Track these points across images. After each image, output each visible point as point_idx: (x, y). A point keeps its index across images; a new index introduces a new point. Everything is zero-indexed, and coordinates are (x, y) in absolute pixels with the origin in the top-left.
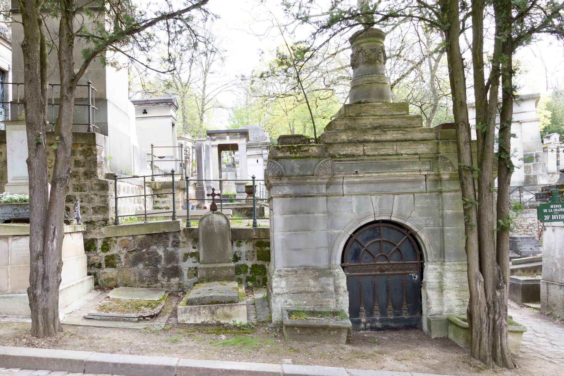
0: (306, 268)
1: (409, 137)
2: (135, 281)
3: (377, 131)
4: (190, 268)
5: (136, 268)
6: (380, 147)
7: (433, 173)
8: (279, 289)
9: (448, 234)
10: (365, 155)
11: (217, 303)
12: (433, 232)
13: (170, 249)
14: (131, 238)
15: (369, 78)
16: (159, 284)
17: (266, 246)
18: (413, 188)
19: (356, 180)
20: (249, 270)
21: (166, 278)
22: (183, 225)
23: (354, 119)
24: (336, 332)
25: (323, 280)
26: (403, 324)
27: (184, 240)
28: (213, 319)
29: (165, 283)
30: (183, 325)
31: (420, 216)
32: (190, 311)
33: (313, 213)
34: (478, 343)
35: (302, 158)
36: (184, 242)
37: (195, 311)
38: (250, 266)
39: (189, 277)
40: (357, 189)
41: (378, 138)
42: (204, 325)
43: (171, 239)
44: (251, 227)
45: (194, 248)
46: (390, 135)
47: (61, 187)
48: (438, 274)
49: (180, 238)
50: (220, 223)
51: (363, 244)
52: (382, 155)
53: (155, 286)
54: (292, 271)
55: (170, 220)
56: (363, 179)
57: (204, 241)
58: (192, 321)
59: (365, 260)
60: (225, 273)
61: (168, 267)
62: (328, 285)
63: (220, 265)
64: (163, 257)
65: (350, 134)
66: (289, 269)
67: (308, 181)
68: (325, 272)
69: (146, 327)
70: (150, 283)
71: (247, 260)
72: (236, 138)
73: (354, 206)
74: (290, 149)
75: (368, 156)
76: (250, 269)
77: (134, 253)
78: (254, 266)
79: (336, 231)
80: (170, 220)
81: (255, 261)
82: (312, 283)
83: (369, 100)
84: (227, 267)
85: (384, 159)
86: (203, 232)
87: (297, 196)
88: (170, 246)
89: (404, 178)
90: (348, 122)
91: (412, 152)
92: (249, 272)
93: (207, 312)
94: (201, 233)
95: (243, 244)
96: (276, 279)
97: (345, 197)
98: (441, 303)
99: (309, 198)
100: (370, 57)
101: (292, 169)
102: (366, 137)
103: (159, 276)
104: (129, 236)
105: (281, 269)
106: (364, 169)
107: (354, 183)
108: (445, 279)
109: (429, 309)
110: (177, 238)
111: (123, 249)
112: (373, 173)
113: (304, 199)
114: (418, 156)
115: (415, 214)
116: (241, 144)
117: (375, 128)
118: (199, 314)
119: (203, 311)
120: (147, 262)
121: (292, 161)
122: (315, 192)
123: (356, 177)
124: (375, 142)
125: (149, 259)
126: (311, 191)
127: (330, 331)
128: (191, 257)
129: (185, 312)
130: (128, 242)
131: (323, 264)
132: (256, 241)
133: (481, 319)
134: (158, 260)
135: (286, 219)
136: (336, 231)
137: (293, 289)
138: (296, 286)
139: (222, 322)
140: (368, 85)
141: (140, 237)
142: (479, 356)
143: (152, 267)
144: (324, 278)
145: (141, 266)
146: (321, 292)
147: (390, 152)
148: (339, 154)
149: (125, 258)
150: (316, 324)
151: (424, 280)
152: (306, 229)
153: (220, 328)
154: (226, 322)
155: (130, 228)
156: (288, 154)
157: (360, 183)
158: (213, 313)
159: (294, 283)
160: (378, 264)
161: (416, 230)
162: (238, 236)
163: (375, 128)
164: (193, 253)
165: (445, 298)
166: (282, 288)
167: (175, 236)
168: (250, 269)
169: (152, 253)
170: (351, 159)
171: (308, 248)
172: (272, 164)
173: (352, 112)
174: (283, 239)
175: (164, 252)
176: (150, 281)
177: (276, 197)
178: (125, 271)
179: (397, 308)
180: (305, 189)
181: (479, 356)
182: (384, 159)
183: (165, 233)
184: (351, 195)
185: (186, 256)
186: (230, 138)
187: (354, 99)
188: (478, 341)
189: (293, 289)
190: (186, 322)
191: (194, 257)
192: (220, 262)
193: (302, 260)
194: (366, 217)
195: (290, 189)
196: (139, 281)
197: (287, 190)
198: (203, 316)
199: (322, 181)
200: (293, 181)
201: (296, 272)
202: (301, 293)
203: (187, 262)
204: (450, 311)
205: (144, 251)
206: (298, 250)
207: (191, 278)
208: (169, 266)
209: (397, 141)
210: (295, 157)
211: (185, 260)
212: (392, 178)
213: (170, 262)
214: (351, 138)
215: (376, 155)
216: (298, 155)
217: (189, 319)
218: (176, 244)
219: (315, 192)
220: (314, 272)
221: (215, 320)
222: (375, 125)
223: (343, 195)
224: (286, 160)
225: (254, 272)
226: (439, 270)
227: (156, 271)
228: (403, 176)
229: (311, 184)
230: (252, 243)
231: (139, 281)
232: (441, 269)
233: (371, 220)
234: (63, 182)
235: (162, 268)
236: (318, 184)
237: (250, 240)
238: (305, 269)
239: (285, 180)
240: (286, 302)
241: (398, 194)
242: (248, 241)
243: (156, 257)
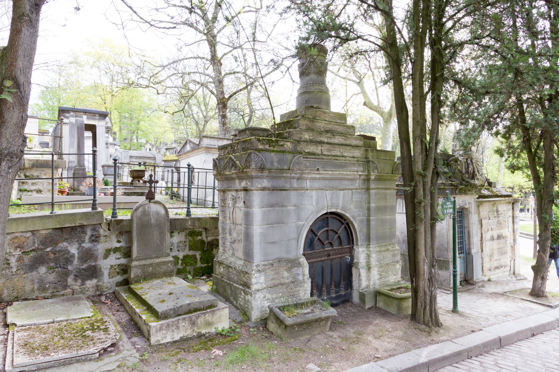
0: (280, 261)
1: (348, 142)
2: (33, 291)
3: (329, 135)
4: (112, 266)
5: (34, 273)
6: (332, 149)
7: (365, 174)
8: (259, 285)
9: (372, 223)
10: (322, 154)
11: (196, 310)
12: (362, 221)
13: (87, 245)
14: (29, 234)
15: (320, 88)
16: (69, 290)
17: (198, 236)
18: (352, 185)
19: (318, 176)
20: (180, 262)
21: (80, 281)
22: (108, 215)
23: (313, 122)
24: (324, 322)
25: (295, 270)
26: (341, 300)
27: (106, 234)
28: (194, 330)
29: (77, 287)
30: (160, 347)
31: (355, 208)
32: (166, 327)
33: (286, 206)
34: (422, 311)
35: (279, 152)
36: (106, 236)
37: (173, 326)
38: (181, 257)
39: (111, 276)
40: (317, 184)
41: (330, 141)
42: (183, 340)
43: (89, 233)
44: (183, 216)
45: (119, 242)
46: (338, 140)
47: (9, 168)
48: (366, 255)
49: (101, 231)
50: (158, 213)
51: (316, 232)
52: (334, 156)
53: (62, 293)
54: (269, 265)
55: (89, 210)
56: (322, 176)
57: (139, 234)
58: (169, 339)
59: (318, 248)
60: (164, 268)
61: (83, 267)
62: (298, 274)
63: (158, 260)
64: (76, 255)
65: (311, 134)
66: (266, 263)
67: (285, 175)
68: (294, 263)
69: (117, 364)
70: (56, 291)
71: (179, 251)
72: (95, 119)
73: (313, 200)
74: (270, 142)
75: (325, 155)
76: (181, 260)
77: (32, 254)
78: (185, 257)
79: (300, 223)
80: (89, 210)
81: (187, 252)
82: (286, 274)
83: (320, 106)
84: (166, 262)
85: (336, 160)
86: (137, 224)
87: (274, 189)
88: (87, 241)
89: (347, 177)
90: (308, 123)
91: (351, 155)
92: (180, 264)
93: (187, 324)
94: (135, 225)
95: (176, 234)
96: (255, 275)
97: (308, 191)
98: (369, 279)
99: (284, 192)
100: (321, 69)
101: (272, 163)
102: (322, 139)
103: (70, 280)
104: (27, 232)
105: (259, 263)
106: (323, 167)
107: (314, 179)
108: (371, 259)
109: (360, 285)
110: (98, 231)
111: (15, 250)
112: (329, 171)
113: (279, 192)
114: (356, 159)
115: (352, 207)
116: (99, 126)
117: (327, 132)
118: (178, 328)
119: (182, 324)
120: (52, 264)
121: (272, 154)
122: (289, 186)
123: (317, 174)
124: (328, 143)
125: (56, 260)
126: (285, 185)
127: (320, 322)
128: (114, 253)
129: (161, 329)
130: (23, 240)
131: (292, 256)
132: (188, 231)
133: (425, 292)
134: (69, 260)
135: (264, 213)
136: (300, 223)
137: (271, 282)
138: (273, 279)
139: (203, 332)
140: (320, 93)
141: (44, 232)
142: (424, 321)
143: (60, 269)
144: (295, 269)
145: (43, 270)
146: (293, 282)
147: (338, 154)
148: (304, 152)
149: (17, 261)
150: (313, 318)
151: (355, 261)
152: (280, 222)
153: (206, 341)
154: (207, 331)
155: (29, 221)
156: (267, 147)
157: (319, 179)
158: (193, 324)
159: (271, 277)
160: (327, 251)
161: (352, 220)
162: (175, 225)
163: (327, 132)
164: (117, 247)
165: (372, 274)
166: (261, 283)
167: (94, 229)
168: (181, 260)
169: (60, 251)
170: (313, 157)
171: (268, 240)
172: (256, 156)
173: (311, 115)
174: (261, 232)
175: (78, 249)
176: (55, 288)
177: (256, 190)
178: (16, 280)
179: (338, 286)
180: (280, 183)
181: (424, 321)
182: (336, 160)
183: (82, 227)
184: (313, 190)
185: (108, 253)
186: (88, 118)
187: (306, 103)
188: (422, 310)
189: (271, 282)
190: (162, 342)
191: (118, 253)
192: (157, 257)
193: (277, 252)
194: (322, 209)
195: (269, 182)
196: (39, 289)
197: (265, 183)
198: (183, 330)
199: (295, 176)
200: (272, 174)
201: (272, 265)
202: (277, 286)
203: (108, 259)
204: (374, 284)
205: (49, 249)
206: (274, 243)
207: (113, 277)
208: (85, 266)
209: (342, 145)
210: (273, 151)
211: (106, 256)
212: (340, 176)
213: (86, 261)
214: (311, 138)
215: (338, 156)
216: (276, 149)
217: (165, 337)
218: (95, 239)
219: (288, 186)
220: (287, 264)
221: (196, 332)
222: (326, 129)
223: (307, 190)
224: (267, 153)
225: (185, 263)
226: (366, 252)
227: (66, 274)
228: (348, 175)
229: (285, 178)
230: (184, 233)
231: (39, 289)
232: (368, 251)
233: (325, 212)
234: (15, 160)
235: (74, 269)
236: (291, 179)
237: (183, 229)
238: (279, 261)
239: (266, 173)
240: (265, 297)
241: (343, 190)
242: (181, 231)
243: (66, 256)
